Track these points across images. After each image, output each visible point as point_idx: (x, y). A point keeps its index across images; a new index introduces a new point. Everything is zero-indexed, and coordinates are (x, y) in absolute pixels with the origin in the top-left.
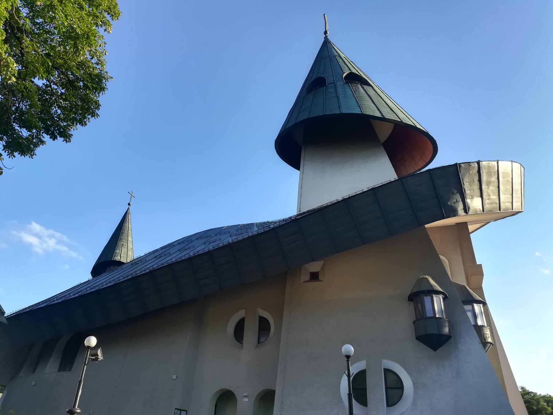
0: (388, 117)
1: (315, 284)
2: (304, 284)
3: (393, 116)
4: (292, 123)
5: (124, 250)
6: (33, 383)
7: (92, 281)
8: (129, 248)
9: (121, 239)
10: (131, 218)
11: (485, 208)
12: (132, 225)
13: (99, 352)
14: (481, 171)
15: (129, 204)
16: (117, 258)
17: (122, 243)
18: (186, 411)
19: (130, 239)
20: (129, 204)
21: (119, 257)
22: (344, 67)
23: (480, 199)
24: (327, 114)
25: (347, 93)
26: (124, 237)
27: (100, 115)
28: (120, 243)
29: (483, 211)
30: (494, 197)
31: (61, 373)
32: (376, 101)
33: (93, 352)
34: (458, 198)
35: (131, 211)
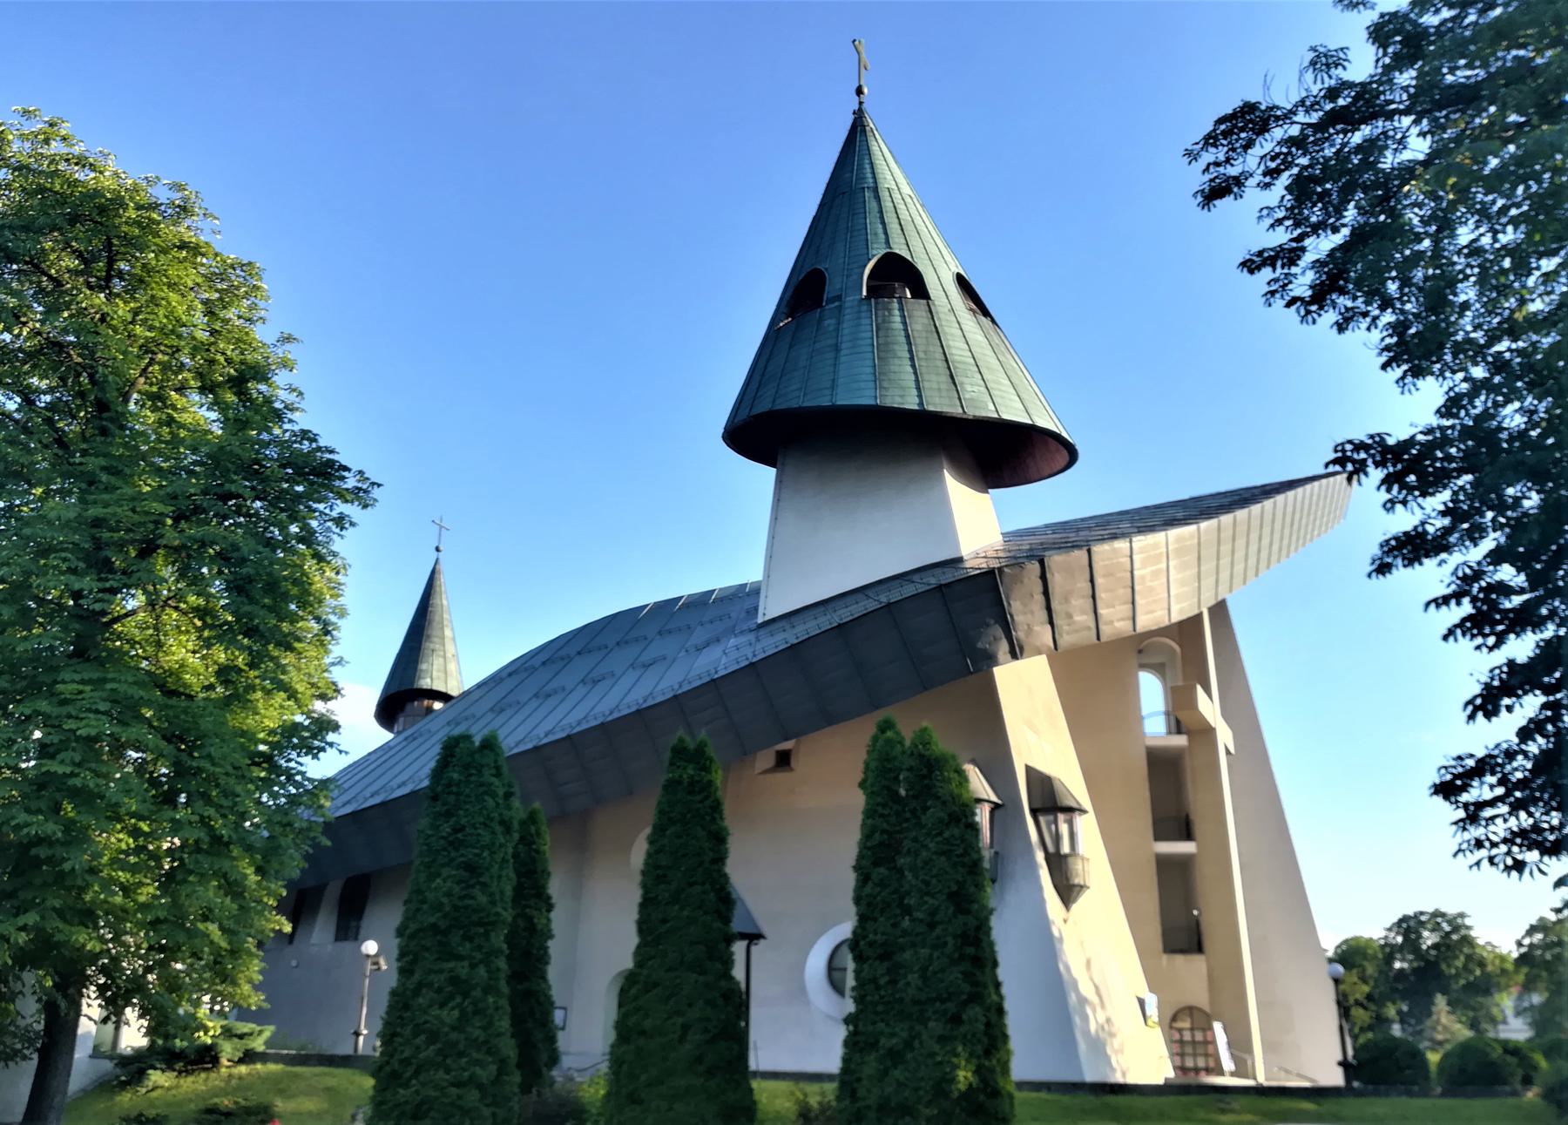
0: (934, 405)
1: (781, 776)
2: (762, 777)
3: (946, 401)
4: (743, 415)
5: (437, 662)
6: (294, 963)
7: (379, 762)
8: (449, 655)
9: (429, 637)
10: (445, 582)
11: (1060, 642)
12: (449, 602)
13: (382, 962)
14: (1048, 576)
15: (438, 549)
16: (426, 683)
17: (432, 646)
18: (565, 1009)
19: (448, 633)
20: (438, 549)
21: (428, 680)
22: (876, 234)
23: (1048, 627)
24: (805, 405)
25: (860, 342)
26: (434, 631)
27: (349, 465)
28: (428, 646)
29: (1056, 648)
30: (1084, 619)
31: (340, 944)
32: (922, 355)
33: (375, 960)
34: (999, 632)
35: (443, 567)
